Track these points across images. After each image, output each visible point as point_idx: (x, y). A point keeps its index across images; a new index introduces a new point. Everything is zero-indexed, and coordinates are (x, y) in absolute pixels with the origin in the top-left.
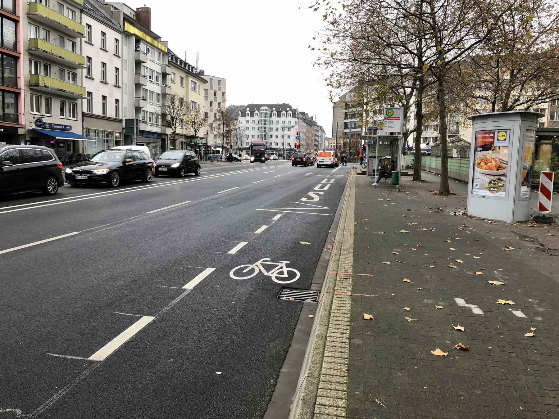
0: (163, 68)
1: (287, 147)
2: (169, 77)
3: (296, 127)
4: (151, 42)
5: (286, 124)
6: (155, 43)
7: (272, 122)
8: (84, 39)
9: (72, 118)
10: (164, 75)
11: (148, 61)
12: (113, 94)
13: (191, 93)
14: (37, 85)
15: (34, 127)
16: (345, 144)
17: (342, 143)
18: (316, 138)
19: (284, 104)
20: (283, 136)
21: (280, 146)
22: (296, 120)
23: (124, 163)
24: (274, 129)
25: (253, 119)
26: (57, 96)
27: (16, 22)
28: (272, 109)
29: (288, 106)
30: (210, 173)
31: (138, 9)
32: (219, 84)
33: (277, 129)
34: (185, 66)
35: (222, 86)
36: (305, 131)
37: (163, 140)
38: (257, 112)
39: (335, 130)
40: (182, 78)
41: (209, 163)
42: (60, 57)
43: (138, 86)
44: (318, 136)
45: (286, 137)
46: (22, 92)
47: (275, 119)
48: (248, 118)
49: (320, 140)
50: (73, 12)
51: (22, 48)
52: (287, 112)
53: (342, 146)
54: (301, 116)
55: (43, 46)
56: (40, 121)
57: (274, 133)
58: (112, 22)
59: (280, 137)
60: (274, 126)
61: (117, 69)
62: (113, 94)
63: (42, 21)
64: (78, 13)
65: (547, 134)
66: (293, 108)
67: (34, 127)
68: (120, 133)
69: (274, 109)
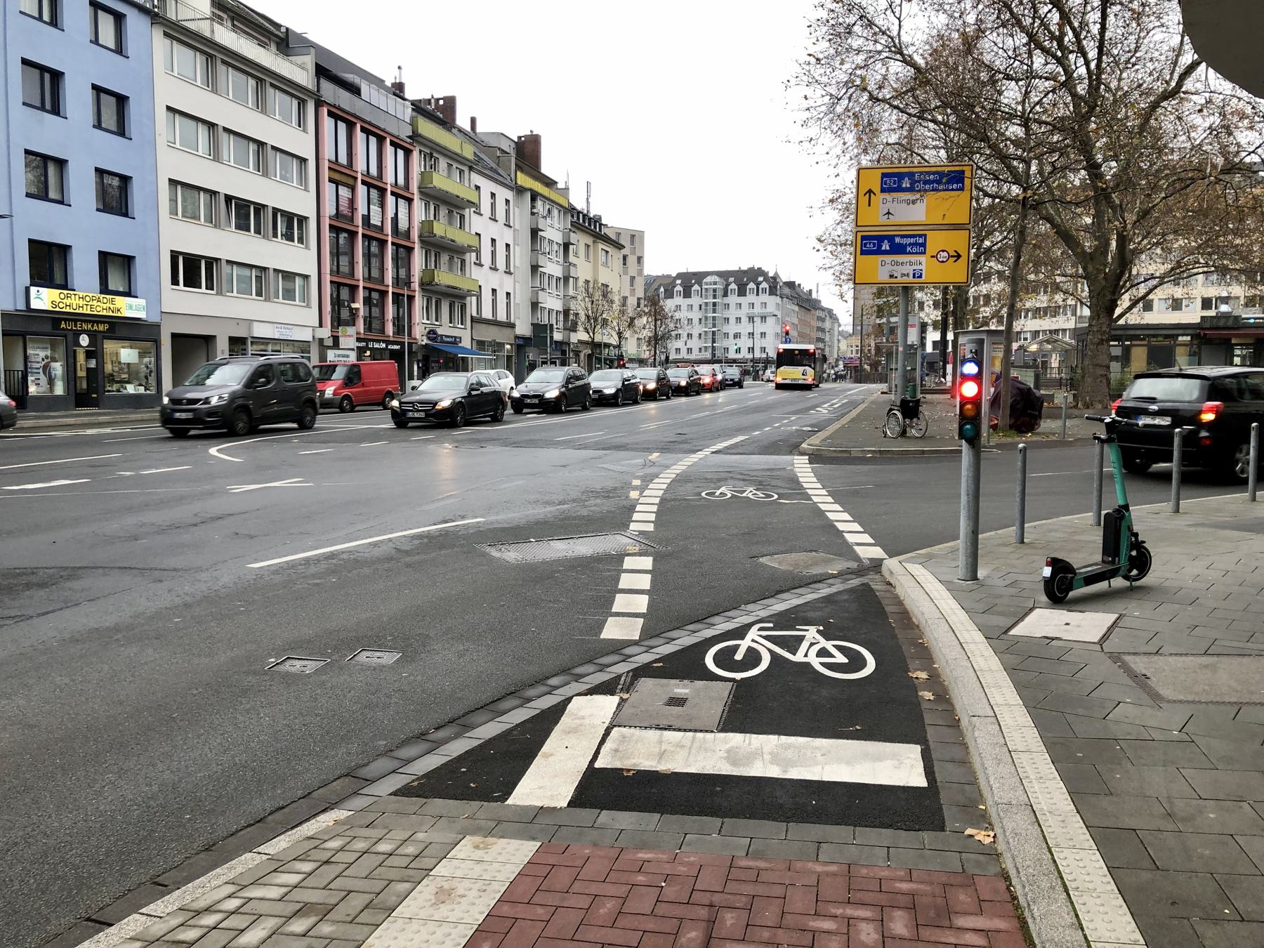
0: (566, 235)
1: (758, 355)
5: (758, 310)
6: (554, 196)
10: (566, 246)
12: (505, 284)
13: (602, 269)
14: (430, 284)
16: (878, 349)
17: (873, 344)
18: (820, 335)
19: (751, 269)
20: (751, 335)
21: (744, 354)
22: (778, 299)
23: (469, 393)
24: (732, 320)
25: (688, 301)
26: (446, 295)
27: (410, 201)
28: (727, 280)
29: (760, 272)
31: (520, 138)
32: (632, 243)
33: (739, 320)
36: (796, 321)
37: (564, 353)
38: (696, 287)
39: (858, 316)
40: (588, 246)
43: (535, 268)
44: (823, 330)
45: (757, 336)
47: (733, 299)
48: (678, 300)
49: (827, 339)
50: (461, 172)
51: (415, 235)
52: (758, 284)
53: (873, 352)
54: (787, 291)
55: (439, 229)
57: (732, 328)
59: (695, 335)
60: (732, 314)
61: (508, 246)
62: (505, 284)
64: (466, 169)
65: (1138, 332)
67: (425, 341)
69: (732, 279)
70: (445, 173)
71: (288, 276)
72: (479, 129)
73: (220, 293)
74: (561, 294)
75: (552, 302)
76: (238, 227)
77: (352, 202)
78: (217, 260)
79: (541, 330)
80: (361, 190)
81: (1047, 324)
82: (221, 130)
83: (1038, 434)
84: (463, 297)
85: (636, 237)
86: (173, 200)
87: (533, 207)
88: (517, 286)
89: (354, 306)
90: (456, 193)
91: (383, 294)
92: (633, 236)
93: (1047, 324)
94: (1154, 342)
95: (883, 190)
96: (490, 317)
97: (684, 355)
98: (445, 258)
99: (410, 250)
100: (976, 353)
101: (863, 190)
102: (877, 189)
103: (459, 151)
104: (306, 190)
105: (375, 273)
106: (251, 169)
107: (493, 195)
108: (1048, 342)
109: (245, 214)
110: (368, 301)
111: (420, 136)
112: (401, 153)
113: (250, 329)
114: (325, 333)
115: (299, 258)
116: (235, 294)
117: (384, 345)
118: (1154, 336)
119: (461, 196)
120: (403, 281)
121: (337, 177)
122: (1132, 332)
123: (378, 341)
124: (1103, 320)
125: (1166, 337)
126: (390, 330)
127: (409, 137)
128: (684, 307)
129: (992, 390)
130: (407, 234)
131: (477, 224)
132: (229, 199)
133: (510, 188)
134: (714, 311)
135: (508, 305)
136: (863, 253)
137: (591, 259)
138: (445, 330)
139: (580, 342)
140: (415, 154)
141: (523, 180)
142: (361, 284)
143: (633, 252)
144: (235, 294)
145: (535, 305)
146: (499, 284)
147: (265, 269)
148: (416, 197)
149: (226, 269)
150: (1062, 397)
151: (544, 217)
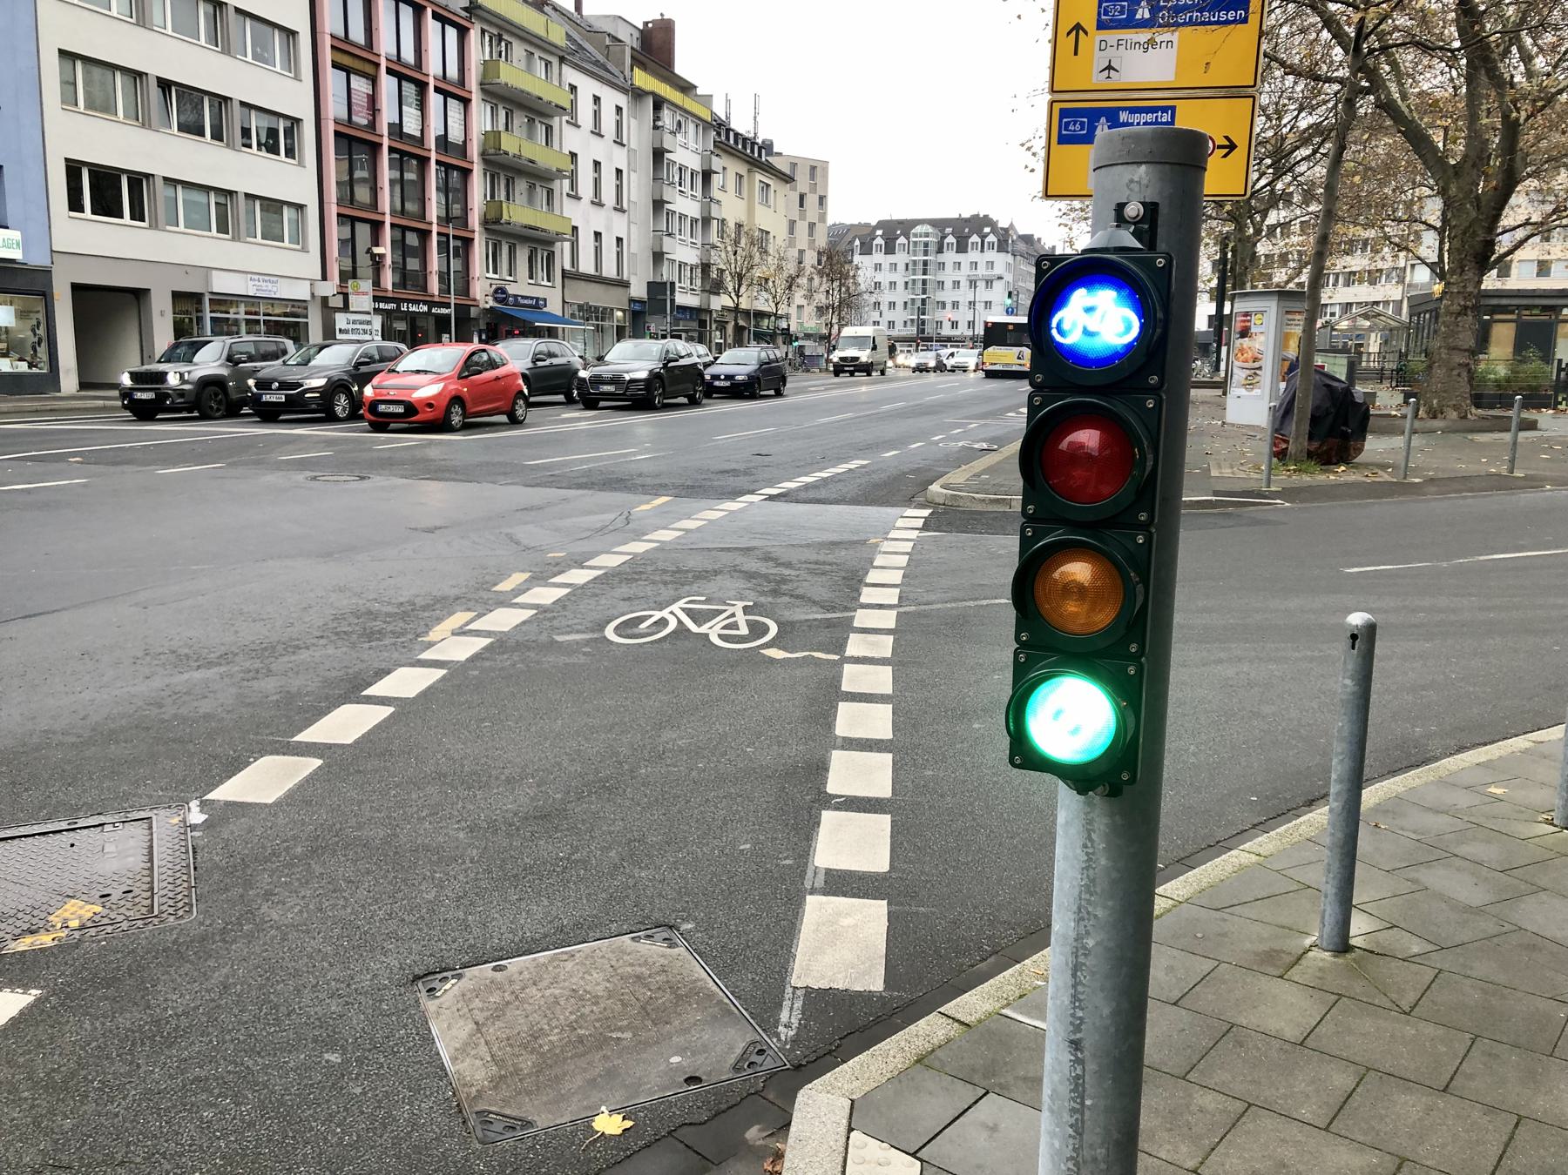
0: (706, 160)
2: (716, 180)
3: (1009, 277)
4: (679, 102)
5: (982, 271)
6: (688, 103)
7: (942, 265)
8: (565, 118)
9: (545, 283)
10: (707, 175)
11: (679, 149)
12: (617, 226)
14: (497, 221)
15: (491, 303)
20: (972, 304)
22: (1009, 258)
24: (948, 285)
25: (891, 258)
26: (524, 239)
27: (466, 102)
28: (942, 231)
29: (987, 221)
30: (809, 392)
31: (646, 24)
32: (812, 177)
33: (956, 284)
34: (744, 147)
35: (818, 180)
37: (702, 324)
38: (902, 240)
41: (800, 375)
42: (532, 162)
43: (658, 205)
45: (980, 307)
46: (476, 236)
47: (950, 257)
48: (878, 257)
50: (548, 64)
51: (474, 151)
52: (983, 237)
54: (1021, 246)
55: (509, 144)
56: (503, 291)
57: (947, 295)
58: (607, 70)
59: (963, 308)
60: (948, 276)
62: (617, 226)
63: (507, 94)
64: (555, 61)
65: (1504, 302)
66: (1000, 225)
67: (491, 303)
68: (624, 311)
69: (949, 230)
70: (523, 65)
71: (273, 206)
72: (585, 12)
73: (154, 226)
74: (699, 241)
75: (684, 252)
76: (182, 128)
77: (373, 100)
78: (148, 176)
79: (659, 290)
80: (388, 84)
81: (1362, 293)
82: (231, 11)
83: (1357, 466)
84: (551, 243)
85: (816, 170)
86: (69, 84)
87: (657, 118)
88: (634, 229)
89: (376, 250)
90: (537, 93)
91: (424, 235)
92: (813, 168)
93: (1362, 293)
94: (1527, 316)
95: (1101, 26)
96: (592, 271)
97: (946, 331)
98: (521, 186)
99: (466, 173)
100: (1148, 224)
101: (1066, 26)
102: (1090, 23)
103: (542, 33)
104: (297, 78)
105: (362, 194)
106: (203, 41)
107: (597, 99)
108: (1366, 316)
109: (195, 109)
110: (400, 245)
111: (480, 7)
112: (452, 33)
113: (207, 280)
114: (329, 289)
115: (291, 179)
116: (182, 227)
117: (425, 308)
118: (1527, 307)
119: (546, 98)
120: (455, 218)
121: (346, 60)
122: (1494, 302)
123: (417, 302)
124: (1469, 275)
125: (1545, 308)
126: (434, 286)
127: (465, 9)
128: (886, 266)
129: (1283, 385)
130: (462, 150)
131: (572, 139)
132: (165, 85)
133: (624, 90)
134: (925, 273)
135: (619, 255)
136: (1062, 140)
137: (745, 194)
138: (521, 287)
139: (724, 308)
140: (474, 35)
141: (642, 79)
142: (388, 220)
143: (813, 188)
144: (182, 227)
145: (658, 257)
146: (603, 225)
147: (230, 193)
148: (476, 97)
149: (161, 189)
150: (1387, 400)
151: (673, 133)
